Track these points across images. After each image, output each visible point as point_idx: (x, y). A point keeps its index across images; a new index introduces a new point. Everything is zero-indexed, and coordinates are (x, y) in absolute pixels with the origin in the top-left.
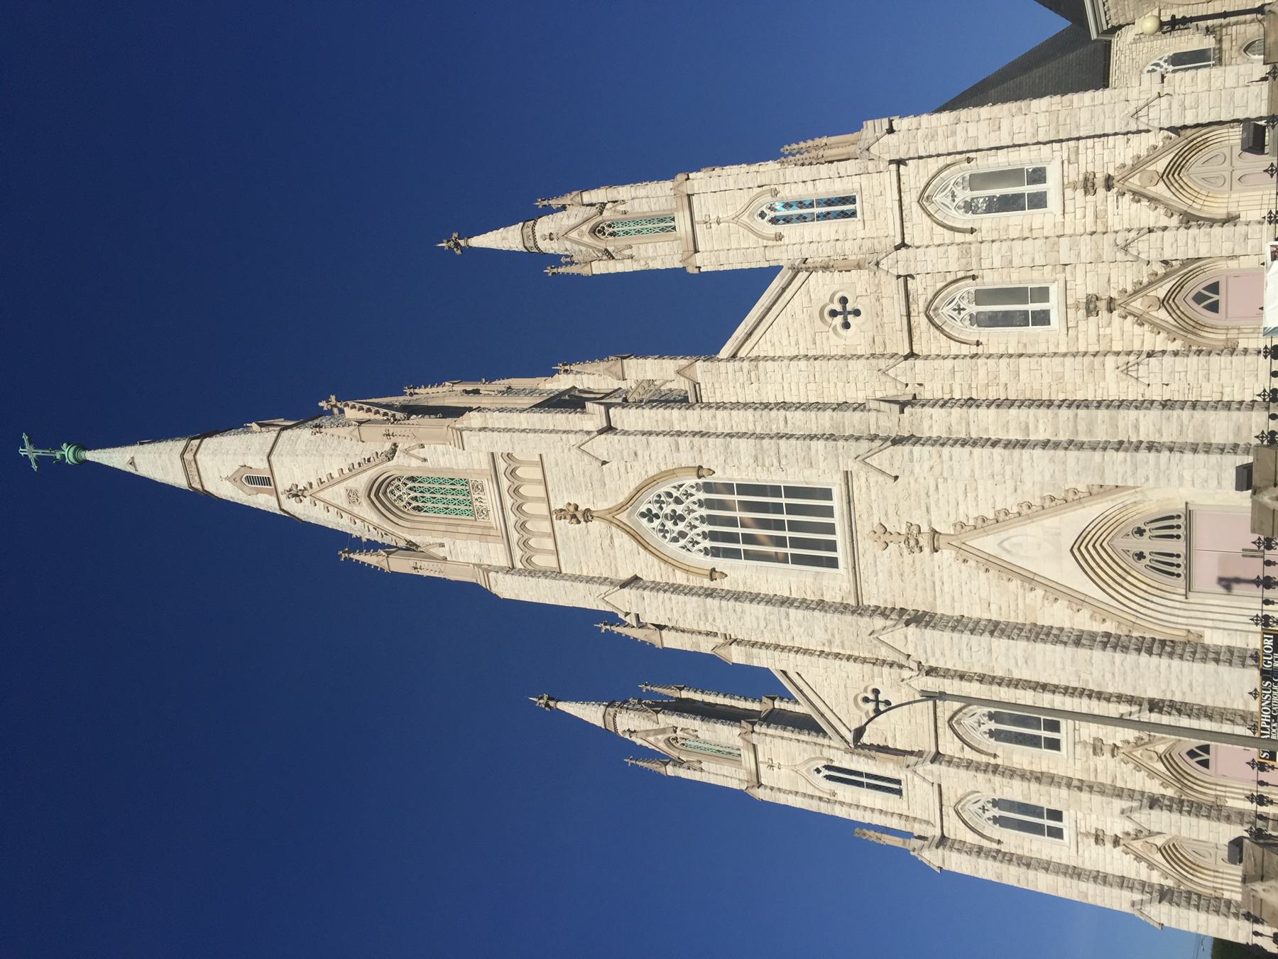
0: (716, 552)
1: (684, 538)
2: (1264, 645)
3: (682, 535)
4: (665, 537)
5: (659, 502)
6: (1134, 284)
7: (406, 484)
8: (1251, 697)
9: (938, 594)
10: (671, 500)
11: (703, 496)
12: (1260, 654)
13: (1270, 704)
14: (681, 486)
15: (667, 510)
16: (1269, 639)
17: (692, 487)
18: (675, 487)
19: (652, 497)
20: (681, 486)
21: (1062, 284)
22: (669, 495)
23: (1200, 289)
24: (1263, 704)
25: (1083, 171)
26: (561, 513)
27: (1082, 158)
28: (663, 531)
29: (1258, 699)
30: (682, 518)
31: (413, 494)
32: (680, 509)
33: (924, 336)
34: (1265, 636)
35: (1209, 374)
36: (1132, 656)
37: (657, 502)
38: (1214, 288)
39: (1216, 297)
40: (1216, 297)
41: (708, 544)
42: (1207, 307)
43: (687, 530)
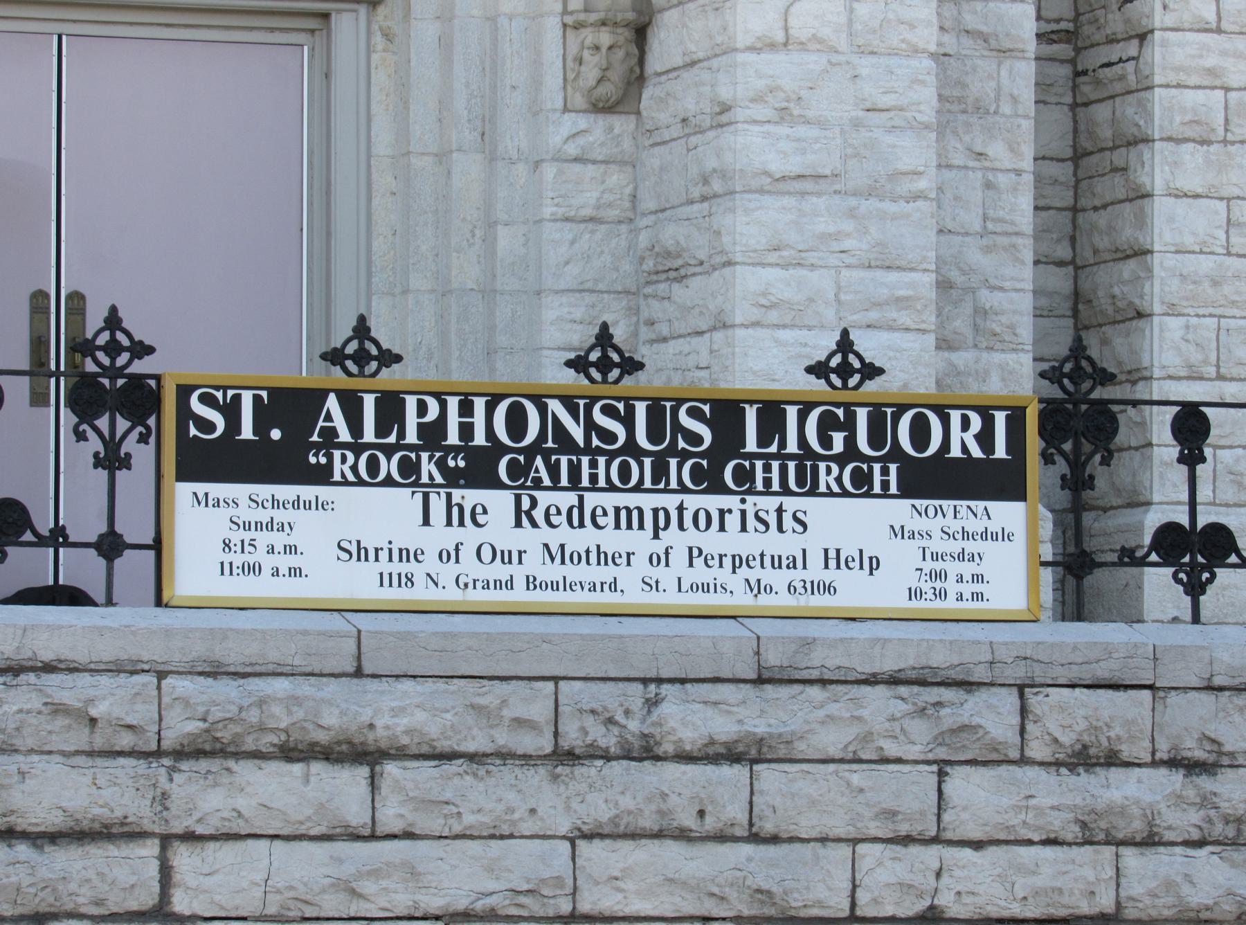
2: (942, 412)
8: (823, 345)
12: (389, 378)
13: (565, 442)
16: (985, 439)
24: (555, 406)
29: (569, 379)
34: (1000, 418)
35: (1204, 142)
36: (176, 894)
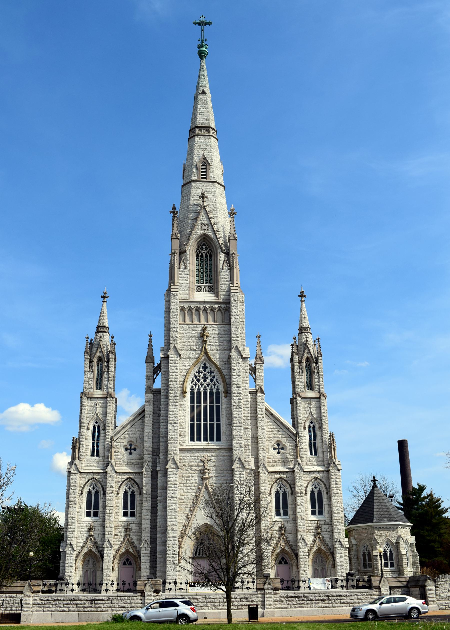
0: (192, 393)
1: (197, 380)
3: (198, 380)
4: (197, 372)
5: (211, 372)
6: (289, 541)
7: (208, 252)
9: (186, 478)
10: (212, 377)
11: (215, 391)
14: (218, 382)
15: (208, 375)
17: (218, 387)
18: (217, 379)
19: (213, 370)
20: (218, 382)
21: (289, 520)
22: (214, 377)
23: (286, 558)
25: (322, 526)
26: (204, 329)
27: (326, 526)
28: (199, 372)
30: (205, 381)
31: (204, 255)
32: (208, 380)
33: (273, 477)
37: (211, 371)
38: (286, 562)
39: (127, 564)
40: (127, 564)
41: (196, 390)
42: (125, 562)
43: (200, 382)
